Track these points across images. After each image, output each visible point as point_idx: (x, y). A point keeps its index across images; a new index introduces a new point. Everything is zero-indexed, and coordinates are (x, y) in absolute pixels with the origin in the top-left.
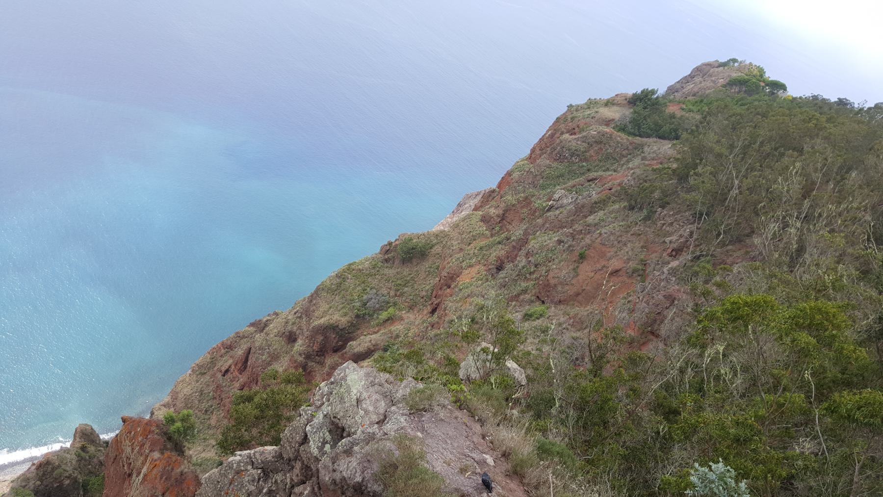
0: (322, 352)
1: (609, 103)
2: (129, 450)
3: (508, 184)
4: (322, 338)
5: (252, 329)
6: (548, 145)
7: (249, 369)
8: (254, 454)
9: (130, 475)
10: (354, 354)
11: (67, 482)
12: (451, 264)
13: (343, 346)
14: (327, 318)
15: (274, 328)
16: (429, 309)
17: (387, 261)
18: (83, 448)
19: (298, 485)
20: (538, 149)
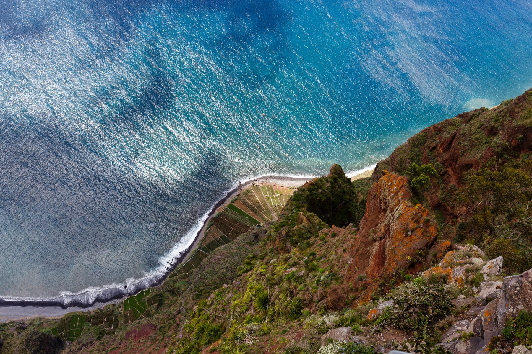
2: (386, 193)
4: (520, 136)
5: (459, 119)
7: (452, 150)
9: (385, 210)
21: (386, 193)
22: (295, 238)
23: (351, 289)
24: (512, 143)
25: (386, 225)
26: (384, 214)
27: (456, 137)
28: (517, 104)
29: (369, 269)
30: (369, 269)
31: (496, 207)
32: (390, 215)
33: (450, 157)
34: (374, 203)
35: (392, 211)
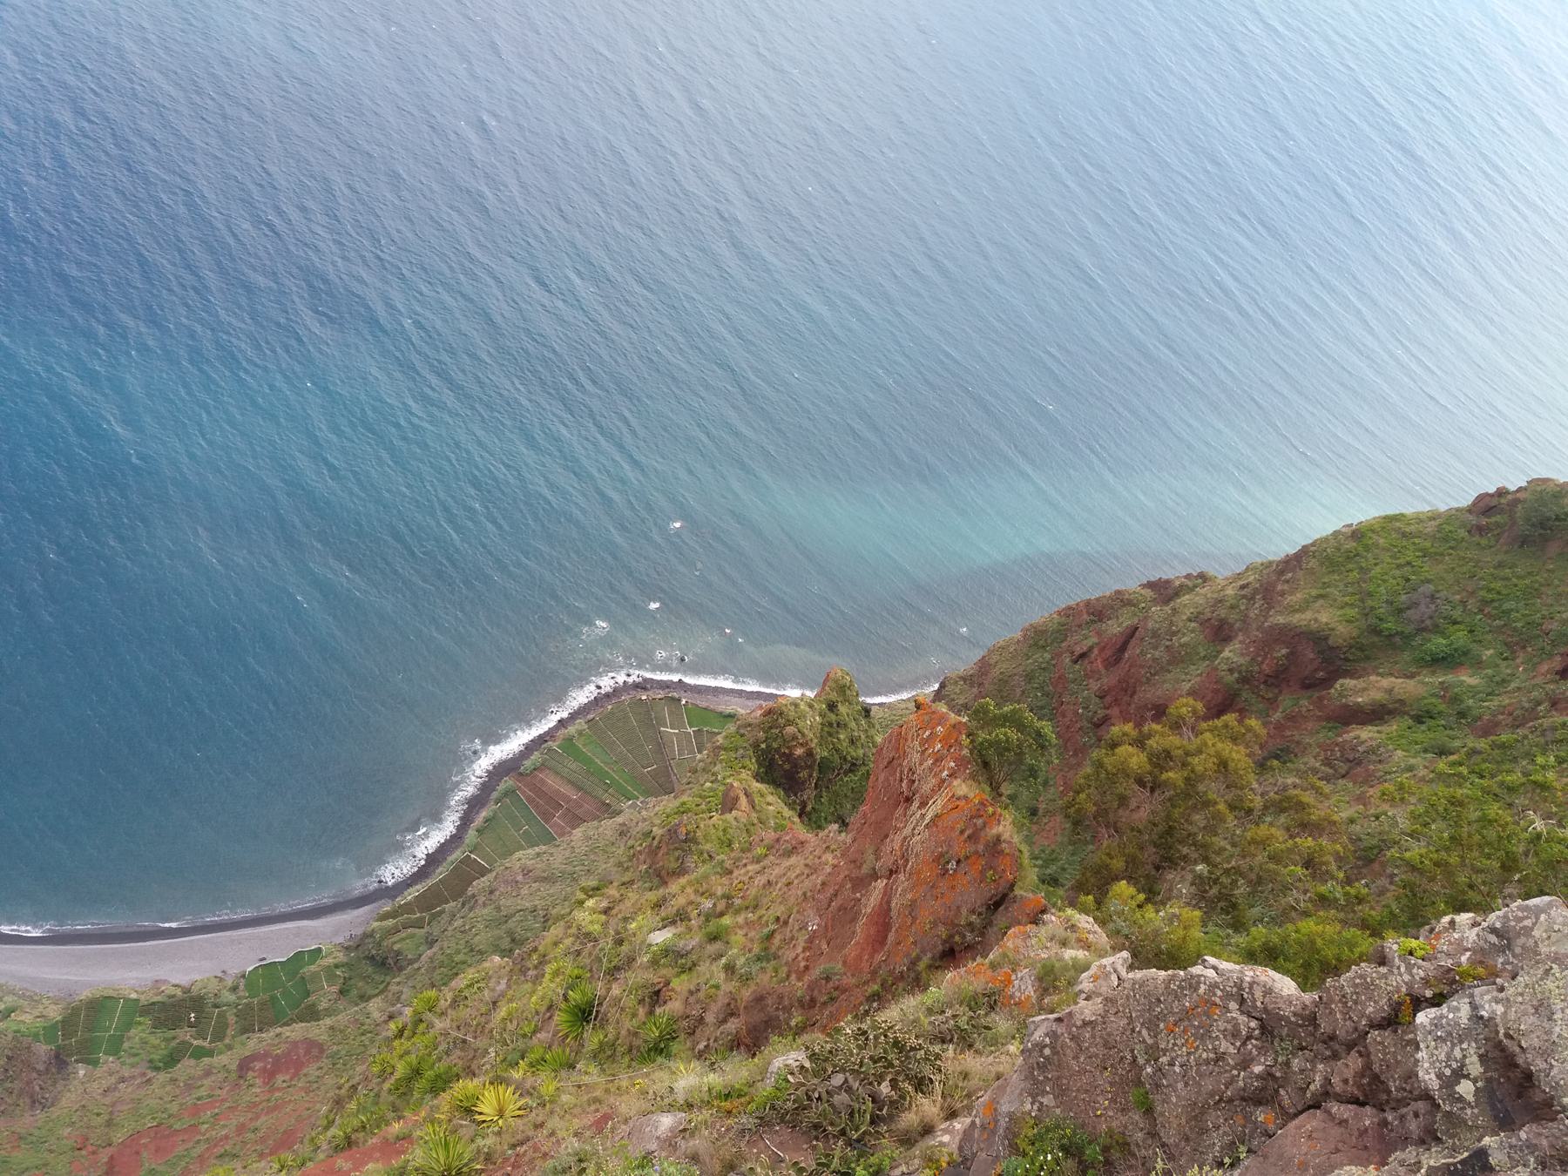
0: (1278, 679)
2: (916, 757)
4: (1284, 651)
5: (1148, 593)
8: (1251, 984)
9: (908, 800)
10: (1346, 706)
11: (799, 751)
13: (1327, 682)
14: (1308, 615)
15: (1188, 603)
17: (1481, 530)
19: (1341, 1099)
22: (708, 847)
23: (800, 1001)
28: (1282, 572)
29: (851, 950)
30: (851, 950)
34: (887, 779)
35: (923, 804)
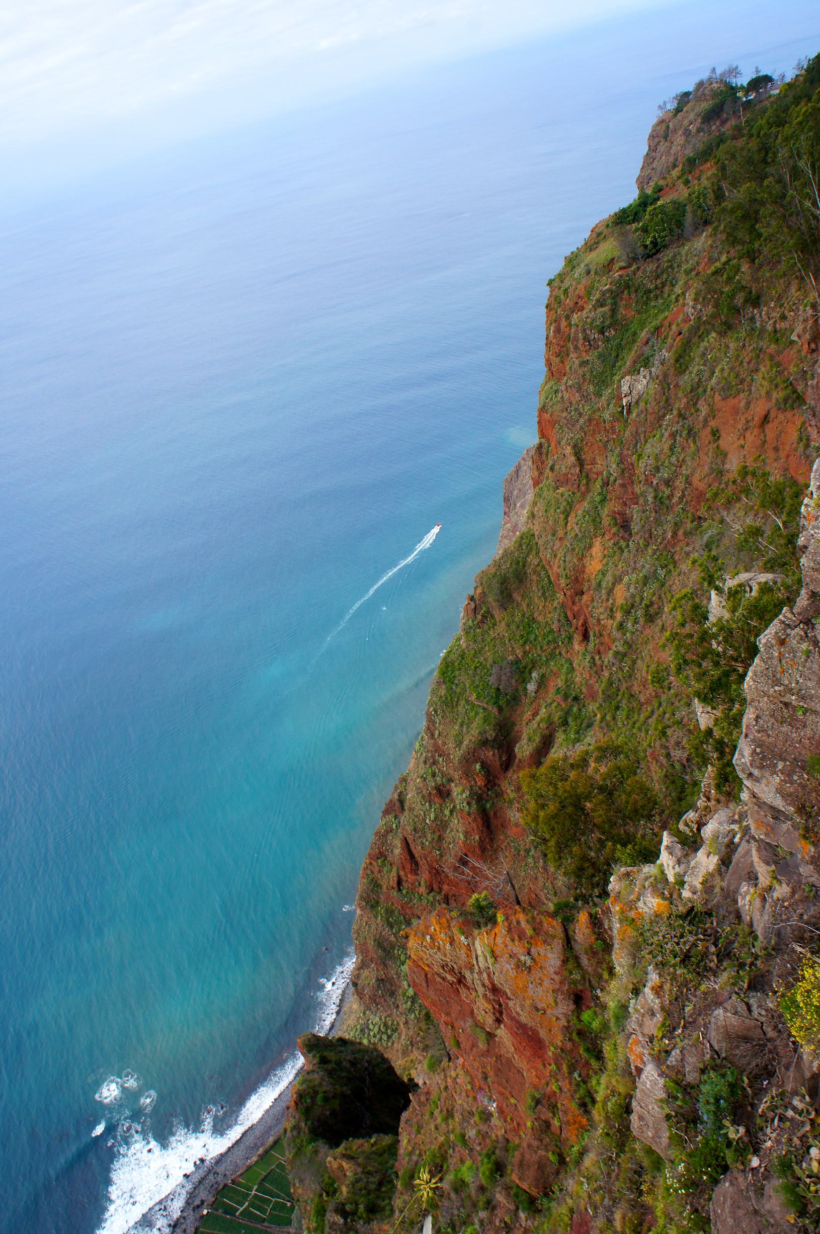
1: (591, 245)
2: (439, 956)
3: (553, 423)
6: (560, 344)
9: (461, 980)
12: (558, 568)
16: (577, 638)
18: (324, 1061)
20: (553, 358)
21: (439, 956)
24: (479, 783)
25: (485, 996)
26: (465, 985)
27: (410, 842)
29: (530, 1076)
31: (569, 844)
32: (476, 976)
33: (430, 872)
35: (471, 968)
